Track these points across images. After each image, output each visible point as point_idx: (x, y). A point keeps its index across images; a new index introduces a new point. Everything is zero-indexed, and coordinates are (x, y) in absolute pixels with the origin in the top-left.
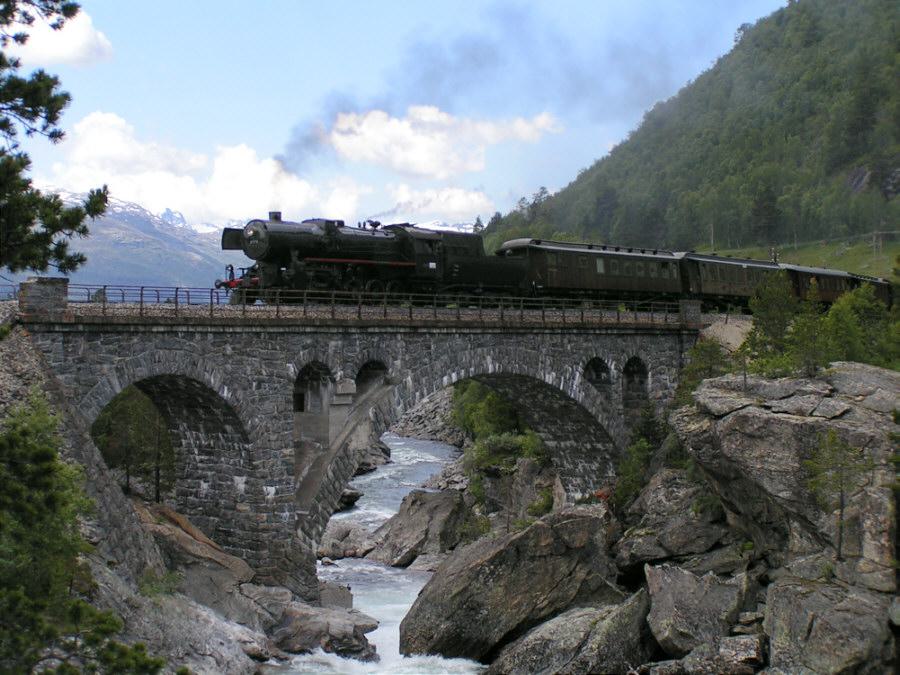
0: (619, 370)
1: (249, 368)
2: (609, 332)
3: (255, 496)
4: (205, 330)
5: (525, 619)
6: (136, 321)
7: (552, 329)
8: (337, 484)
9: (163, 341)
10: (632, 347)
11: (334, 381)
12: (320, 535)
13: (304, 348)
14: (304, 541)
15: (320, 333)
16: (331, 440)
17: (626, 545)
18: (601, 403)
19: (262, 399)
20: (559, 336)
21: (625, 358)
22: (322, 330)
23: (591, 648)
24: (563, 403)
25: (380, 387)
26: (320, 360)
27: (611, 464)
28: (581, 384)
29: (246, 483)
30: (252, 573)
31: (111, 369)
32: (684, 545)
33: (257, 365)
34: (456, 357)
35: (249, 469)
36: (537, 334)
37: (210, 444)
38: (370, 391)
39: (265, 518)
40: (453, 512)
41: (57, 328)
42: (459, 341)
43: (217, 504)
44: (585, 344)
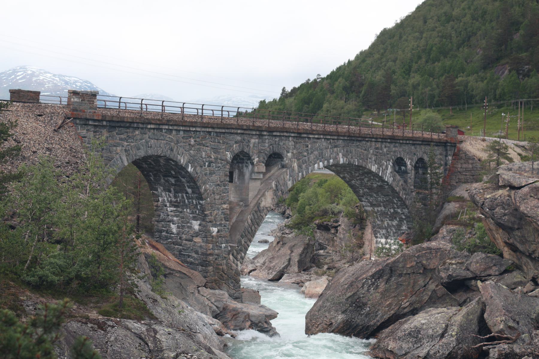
0: (412, 166)
1: (204, 153)
2: (408, 142)
3: (204, 232)
4: (179, 129)
5: (393, 315)
6: (138, 121)
7: (376, 138)
8: (253, 228)
9: (154, 134)
10: (421, 152)
11: (252, 164)
12: (242, 258)
13: (236, 143)
14: (234, 262)
15: (246, 134)
16: (250, 200)
17: (445, 269)
18: (402, 185)
19: (211, 174)
20: (379, 143)
21: (415, 159)
22: (247, 132)
23: (451, 335)
24: (379, 184)
25: (279, 169)
26: (245, 151)
27: (405, 222)
28: (391, 172)
29: (200, 225)
30: (204, 281)
31: (122, 150)
32: (485, 270)
33: (209, 152)
34: (322, 153)
35: (202, 216)
36: (367, 141)
37: (177, 201)
38: (272, 172)
39: (211, 247)
40: (304, 249)
41: (91, 123)
42: (324, 143)
43: (180, 238)
44: (394, 149)
